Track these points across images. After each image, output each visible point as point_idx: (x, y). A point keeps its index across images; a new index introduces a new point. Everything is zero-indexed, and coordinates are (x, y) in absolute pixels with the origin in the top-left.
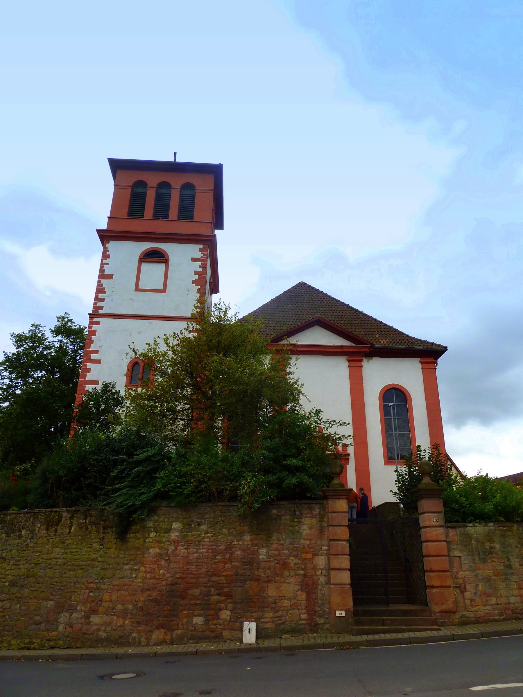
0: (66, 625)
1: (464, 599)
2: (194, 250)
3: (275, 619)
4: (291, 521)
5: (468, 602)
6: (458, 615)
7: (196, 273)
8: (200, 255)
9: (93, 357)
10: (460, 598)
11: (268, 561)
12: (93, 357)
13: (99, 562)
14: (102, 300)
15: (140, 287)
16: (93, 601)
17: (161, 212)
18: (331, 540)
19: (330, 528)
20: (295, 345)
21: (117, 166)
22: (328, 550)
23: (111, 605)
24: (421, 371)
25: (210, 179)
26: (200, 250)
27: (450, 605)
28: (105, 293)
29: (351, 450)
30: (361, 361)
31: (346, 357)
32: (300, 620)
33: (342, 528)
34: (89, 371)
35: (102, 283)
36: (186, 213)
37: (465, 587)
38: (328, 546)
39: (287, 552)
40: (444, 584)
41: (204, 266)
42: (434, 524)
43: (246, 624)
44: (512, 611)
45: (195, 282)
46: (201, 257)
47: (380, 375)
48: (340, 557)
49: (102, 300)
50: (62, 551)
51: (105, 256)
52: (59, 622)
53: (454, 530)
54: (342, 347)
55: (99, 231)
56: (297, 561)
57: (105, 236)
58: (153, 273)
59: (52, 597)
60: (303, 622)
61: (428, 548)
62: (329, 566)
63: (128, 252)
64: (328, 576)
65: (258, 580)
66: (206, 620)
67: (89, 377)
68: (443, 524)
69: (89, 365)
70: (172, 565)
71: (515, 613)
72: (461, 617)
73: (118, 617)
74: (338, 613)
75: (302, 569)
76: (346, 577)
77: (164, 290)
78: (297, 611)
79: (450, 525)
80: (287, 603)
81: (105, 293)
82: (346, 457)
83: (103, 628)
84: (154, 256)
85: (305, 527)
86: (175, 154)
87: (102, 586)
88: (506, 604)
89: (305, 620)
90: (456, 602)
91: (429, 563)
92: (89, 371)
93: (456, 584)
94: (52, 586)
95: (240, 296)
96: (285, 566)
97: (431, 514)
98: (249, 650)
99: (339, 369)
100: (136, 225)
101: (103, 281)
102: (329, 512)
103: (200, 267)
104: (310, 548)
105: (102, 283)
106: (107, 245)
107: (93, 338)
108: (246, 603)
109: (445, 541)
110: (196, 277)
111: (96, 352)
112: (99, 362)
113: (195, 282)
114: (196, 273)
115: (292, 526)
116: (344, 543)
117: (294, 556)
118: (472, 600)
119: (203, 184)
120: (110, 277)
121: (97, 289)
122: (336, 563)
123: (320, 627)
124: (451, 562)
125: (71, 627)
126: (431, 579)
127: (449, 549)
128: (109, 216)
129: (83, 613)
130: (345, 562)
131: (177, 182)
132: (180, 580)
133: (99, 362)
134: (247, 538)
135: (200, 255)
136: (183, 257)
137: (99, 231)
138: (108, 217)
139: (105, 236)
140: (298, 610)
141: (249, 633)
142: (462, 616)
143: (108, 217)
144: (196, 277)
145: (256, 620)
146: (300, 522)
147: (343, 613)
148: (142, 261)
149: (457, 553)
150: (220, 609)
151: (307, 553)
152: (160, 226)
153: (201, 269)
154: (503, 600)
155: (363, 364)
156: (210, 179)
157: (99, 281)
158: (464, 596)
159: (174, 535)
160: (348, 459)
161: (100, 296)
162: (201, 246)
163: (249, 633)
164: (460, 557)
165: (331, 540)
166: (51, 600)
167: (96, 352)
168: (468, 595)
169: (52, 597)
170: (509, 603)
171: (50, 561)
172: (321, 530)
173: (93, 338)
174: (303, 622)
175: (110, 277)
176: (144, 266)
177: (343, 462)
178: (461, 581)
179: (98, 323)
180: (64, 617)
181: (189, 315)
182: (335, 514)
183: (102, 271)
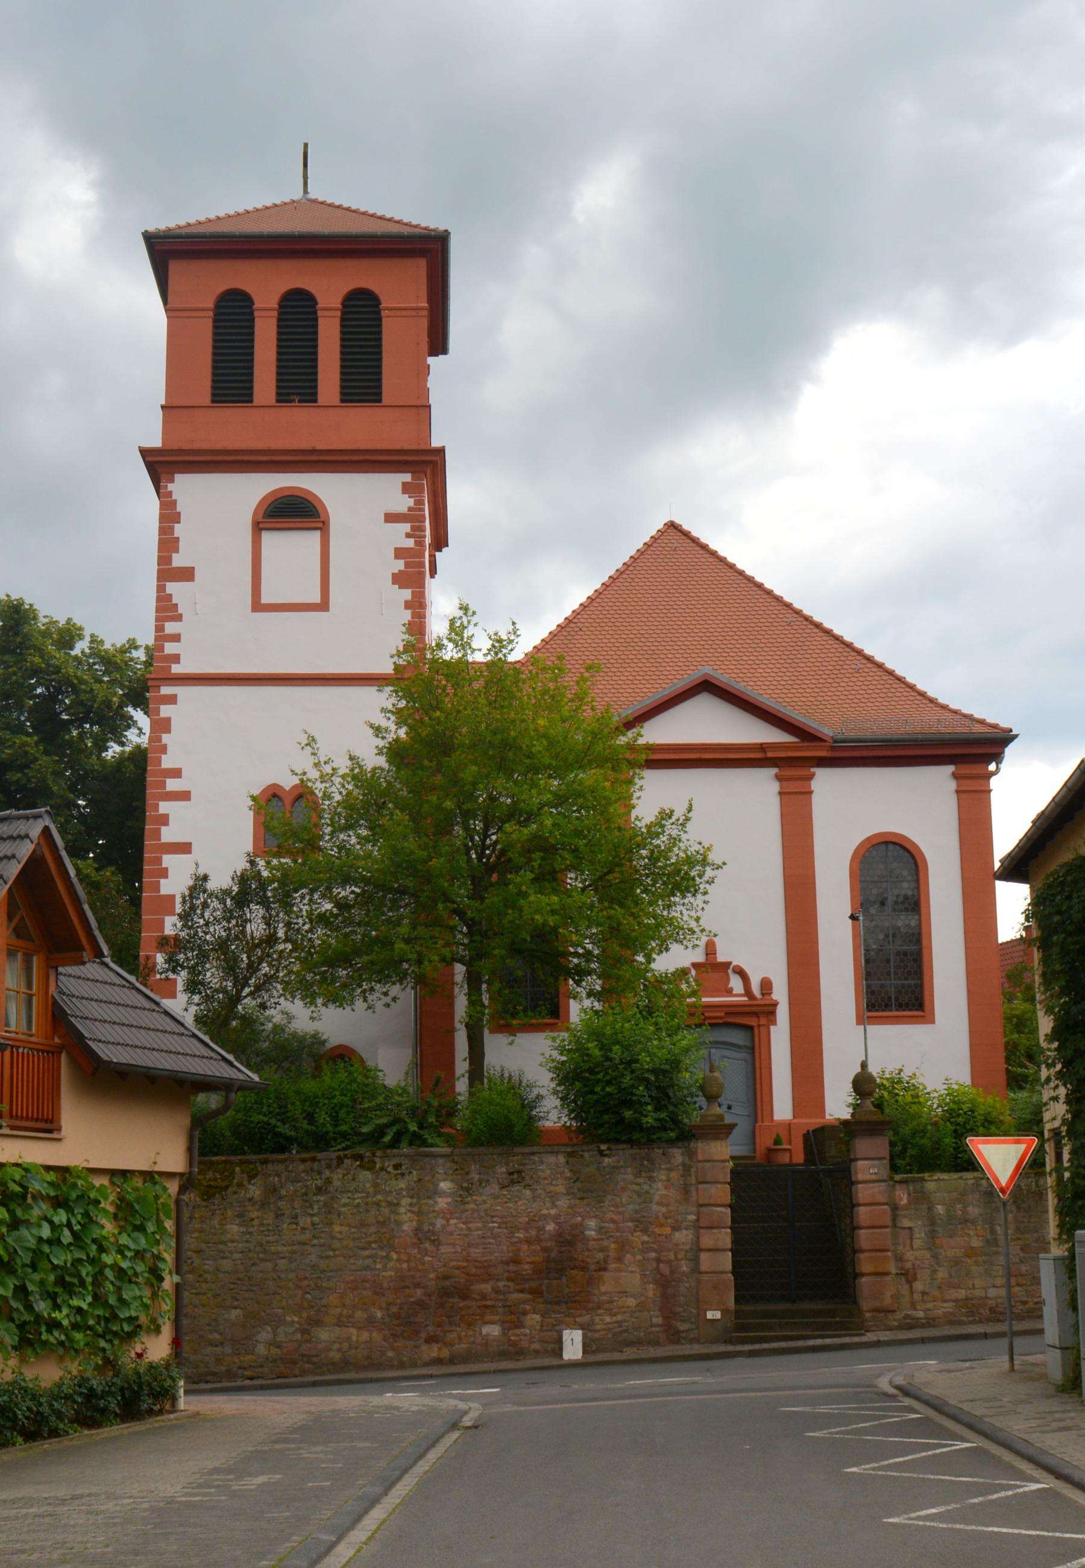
0: (270, 1344)
1: (912, 1292)
2: (388, 490)
3: (610, 1326)
4: (636, 1177)
5: (917, 1297)
6: (899, 1315)
7: (399, 553)
8: (403, 503)
9: (172, 785)
10: (905, 1290)
11: (598, 1240)
12: (172, 785)
13: (313, 1246)
14: (176, 638)
15: (265, 600)
16: (313, 1307)
17: (296, 384)
18: (701, 1206)
19: (700, 1186)
20: (649, 748)
21: (167, 252)
22: (698, 1220)
23: (345, 1312)
24: (954, 797)
25: (419, 268)
26: (406, 488)
27: (887, 1301)
28: (179, 618)
29: (780, 994)
30: (811, 777)
31: (774, 771)
32: (652, 1326)
33: (719, 1186)
34: (164, 820)
35: (168, 591)
36: (363, 383)
37: (915, 1274)
38: (698, 1214)
39: (630, 1224)
40: (880, 1270)
41: (416, 533)
42: (874, 1177)
43: (567, 1335)
44: (991, 1309)
45: (399, 579)
46: (410, 509)
47: (852, 807)
48: (715, 1231)
49: (176, 638)
50: (243, 1229)
51: (169, 516)
52: (257, 1341)
53: (904, 1186)
54: (762, 747)
55: (145, 452)
56: (646, 1238)
57: (161, 465)
58: (291, 553)
59: (236, 1303)
60: (657, 1329)
61: (863, 1214)
62: (698, 1246)
63: (222, 504)
64: (696, 1260)
65: (583, 1269)
66: (503, 1329)
67: (168, 835)
68: (885, 1177)
69: (164, 807)
70: (443, 1249)
71: (995, 1312)
72: (904, 1318)
73: (359, 1329)
74: (710, 1315)
75: (655, 1251)
76: (726, 1261)
77: (258, 606)
78: (646, 1313)
79: (897, 1177)
80: (632, 1302)
81: (179, 618)
82: (769, 1011)
83: (336, 1346)
84: (291, 512)
85: (660, 1185)
86: (306, 145)
87: (325, 1285)
88: (982, 1298)
89: (658, 1326)
90: (896, 1297)
91: (864, 1238)
92: (164, 820)
93: (902, 1269)
94: (232, 1286)
95: (514, 590)
96: (623, 1246)
97: (866, 1162)
98: (573, 1365)
99: (760, 788)
100: (233, 427)
101: (171, 587)
102: (699, 1161)
103: (408, 536)
104: (667, 1218)
105: (168, 591)
106: (171, 487)
107: (165, 738)
108: (566, 1303)
109: (886, 1204)
110: (400, 565)
111: (176, 773)
112: (185, 796)
113: (399, 579)
114: (399, 553)
115: (637, 1184)
116: (722, 1209)
117: (641, 1231)
118: (923, 1293)
119: (397, 287)
120: (187, 574)
121: (158, 610)
122: (707, 1240)
123: (683, 1335)
124: (895, 1236)
125: (279, 1347)
126: (865, 1264)
127: (895, 1219)
128: (163, 403)
129: (297, 1326)
130: (725, 1238)
131: (329, 286)
132: (457, 1272)
133: (185, 796)
134: (563, 1203)
135: (403, 503)
136: (362, 506)
137: (145, 452)
138: (163, 407)
139: (161, 465)
140: (648, 1311)
141: (573, 1344)
142: (907, 1316)
143: (163, 407)
144: (400, 565)
145: (582, 1327)
146: (651, 1178)
147: (717, 1315)
148: (261, 529)
149: (906, 1223)
150: (525, 1313)
151: (661, 1225)
152: (300, 427)
153: (410, 543)
154: (979, 1293)
155: (815, 785)
156: (419, 268)
157: (161, 589)
158: (911, 1287)
159: (442, 1203)
160: (773, 1013)
161: (170, 628)
162: (407, 477)
163: (573, 1344)
164: (910, 1228)
165: (701, 1206)
166: (235, 1308)
167: (176, 773)
168: (918, 1286)
169: (236, 1303)
170: (986, 1297)
171: (221, 1246)
172: (686, 1191)
173: (165, 738)
174: (657, 1329)
175: (187, 574)
176: (269, 539)
177: (763, 1021)
178: (909, 1265)
179: (172, 700)
180: (265, 1335)
181: (388, 669)
182: (708, 1164)
183: (164, 559)
